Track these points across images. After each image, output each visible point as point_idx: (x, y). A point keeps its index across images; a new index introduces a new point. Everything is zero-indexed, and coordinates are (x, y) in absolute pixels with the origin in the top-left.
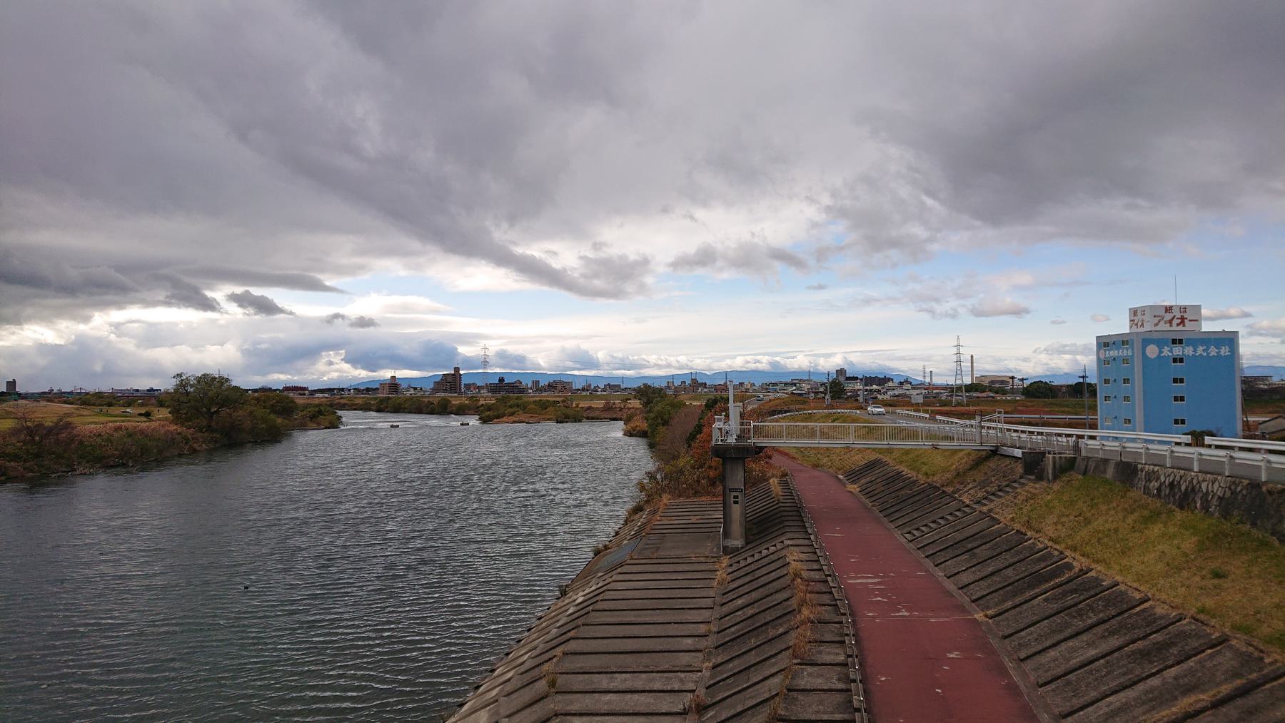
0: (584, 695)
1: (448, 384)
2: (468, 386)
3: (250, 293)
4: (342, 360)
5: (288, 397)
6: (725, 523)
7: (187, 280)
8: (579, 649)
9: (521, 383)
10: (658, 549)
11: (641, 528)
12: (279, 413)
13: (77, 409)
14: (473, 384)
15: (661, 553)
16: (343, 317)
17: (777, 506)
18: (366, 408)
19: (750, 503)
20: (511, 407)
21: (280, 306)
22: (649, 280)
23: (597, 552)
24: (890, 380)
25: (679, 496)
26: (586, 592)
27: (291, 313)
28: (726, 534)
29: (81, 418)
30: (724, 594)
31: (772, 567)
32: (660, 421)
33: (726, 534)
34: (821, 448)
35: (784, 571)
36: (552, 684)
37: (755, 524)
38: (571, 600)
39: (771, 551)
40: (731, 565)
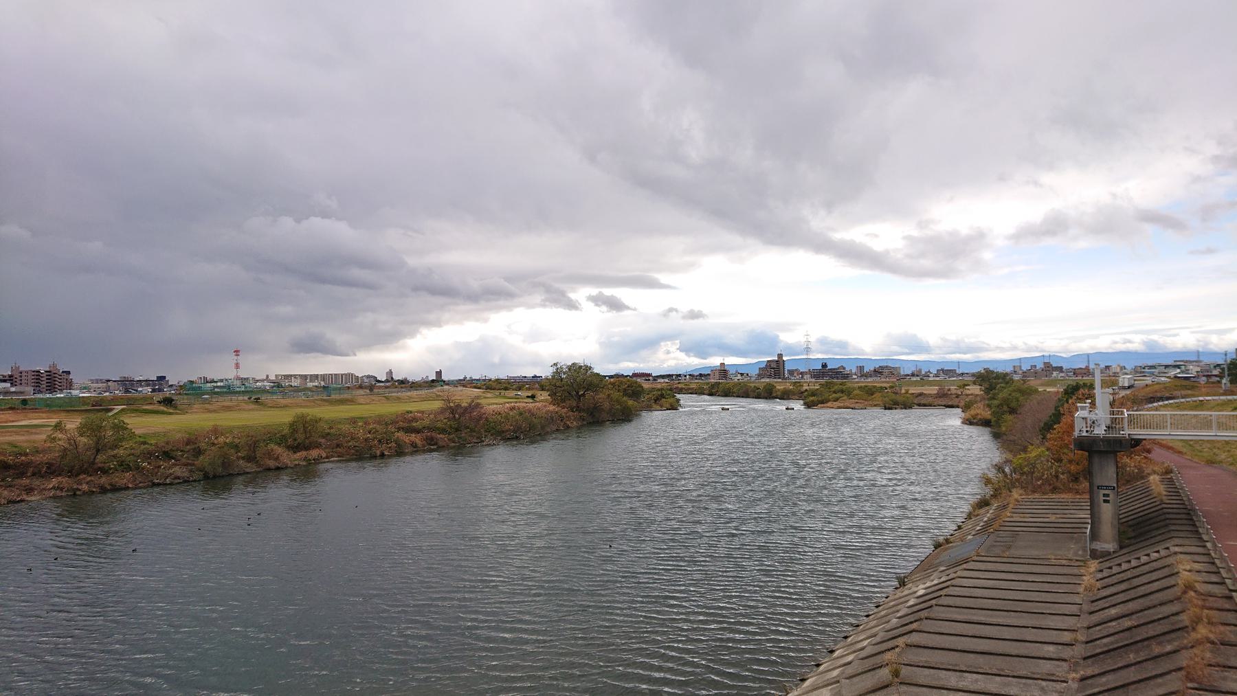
0: (930, 690)
1: (772, 370)
2: (791, 372)
3: (603, 294)
4: (678, 349)
5: (636, 382)
6: (1092, 524)
7: (557, 285)
8: (923, 643)
9: (844, 368)
10: (1009, 548)
11: (988, 524)
12: (630, 396)
13: (484, 393)
14: (796, 370)
15: (1014, 552)
16: (676, 310)
17: (1159, 507)
18: (699, 392)
19: (1125, 503)
20: (835, 392)
21: (626, 304)
22: (987, 255)
23: (937, 546)
25: (1034, 492)
26: (928, 584)
27: (635, 309)
28: (1094, 536)
29: (487, 400)
30: (1093, 602)
31: (1154, 576)
32: (1005, 408)
33: (1094, 536)
34: (1218, 442)
35: (1171, 581)
36: (896, 674)
37: (1130, 526)
38: (910, 591)
39: (1153, 558)
40: (1101, 571)
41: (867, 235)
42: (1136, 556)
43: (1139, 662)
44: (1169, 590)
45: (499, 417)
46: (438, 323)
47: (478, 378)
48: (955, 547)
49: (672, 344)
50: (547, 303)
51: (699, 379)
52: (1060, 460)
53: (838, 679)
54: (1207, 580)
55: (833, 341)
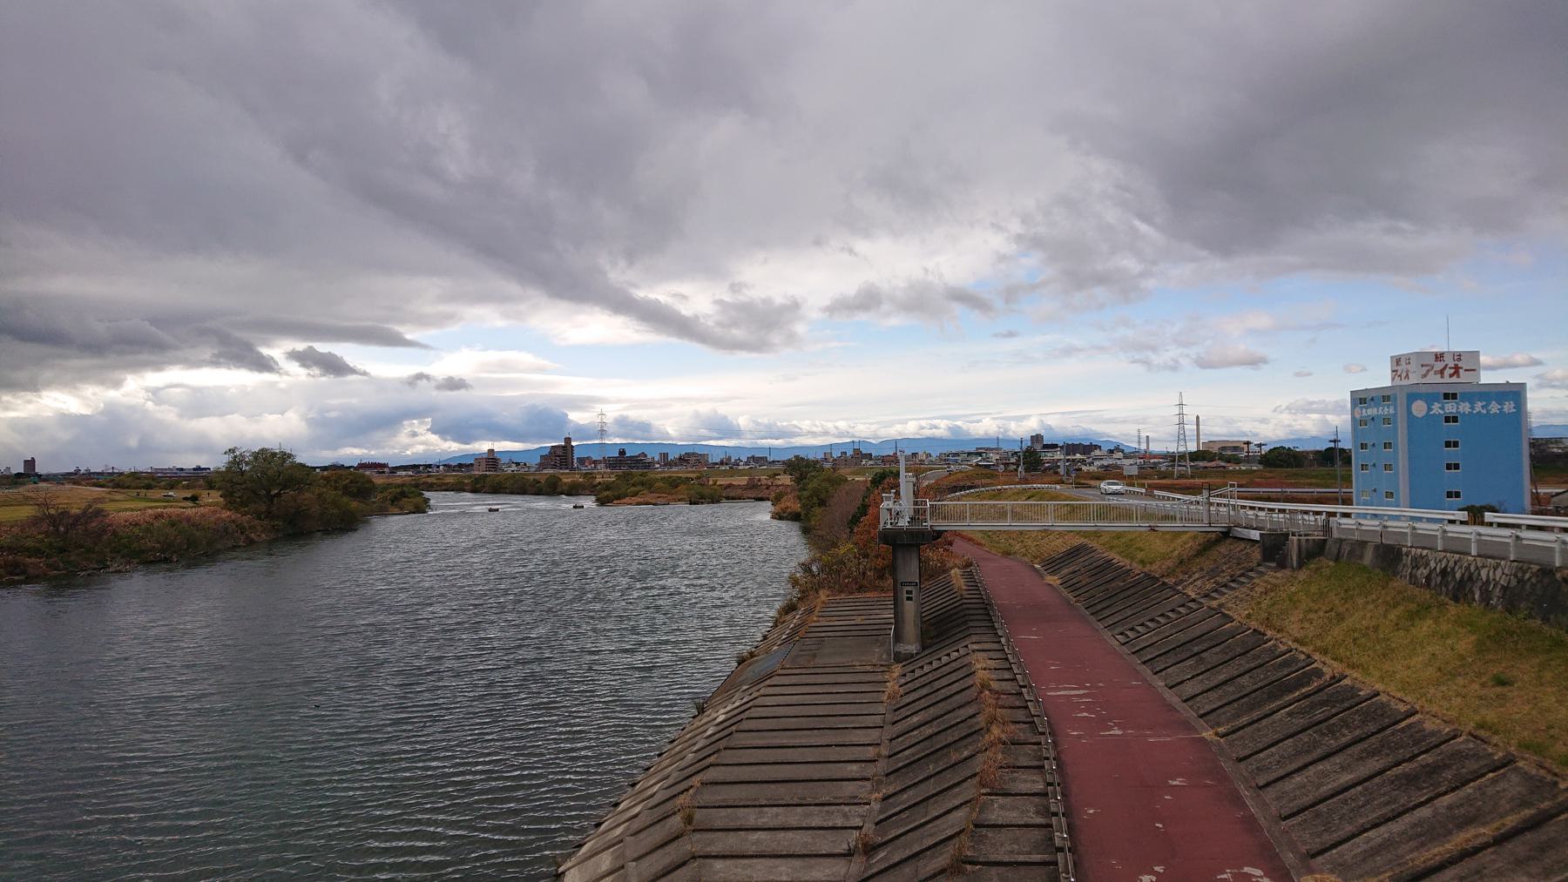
2: (582, 461)
3: (314, 349)
4: (428, 430)
5: (364, 476)
7: (237, 334)
8: (721, 778)
9: (646, 456)
10: (814, 656)
11: (795, 631)
13: (109, 493)
15: (819, 661)
16: (427, 377)
17: (960, 602)
18: (458, 488)
19: (927, 600)
21: (351, 365)
22: (800, 328)
24: (1098, 447)
26: (728, 708)
27: (365, 374)
28: (898, 638)
29: (116, 503)
30: (896, 710)
31: (954, 677)
33: (898, 638)
34: (1015, 532)
36: (689, 820)
38: (710, 718)
39: (953, 658)
40: (905, 675)
41: (675, 295)
42: (937, 657)
43: (938, 773)
44: (966, 691)
45: (136, 530)
46: (33, 386)
47: (100, 471)
48: (760, 660)
49: (420, 423)
50: (222, 360)
51: (458, 471)
52: (866, 556)
53: (621, 838)
54: (1001, 677)
55: (633, 422)
